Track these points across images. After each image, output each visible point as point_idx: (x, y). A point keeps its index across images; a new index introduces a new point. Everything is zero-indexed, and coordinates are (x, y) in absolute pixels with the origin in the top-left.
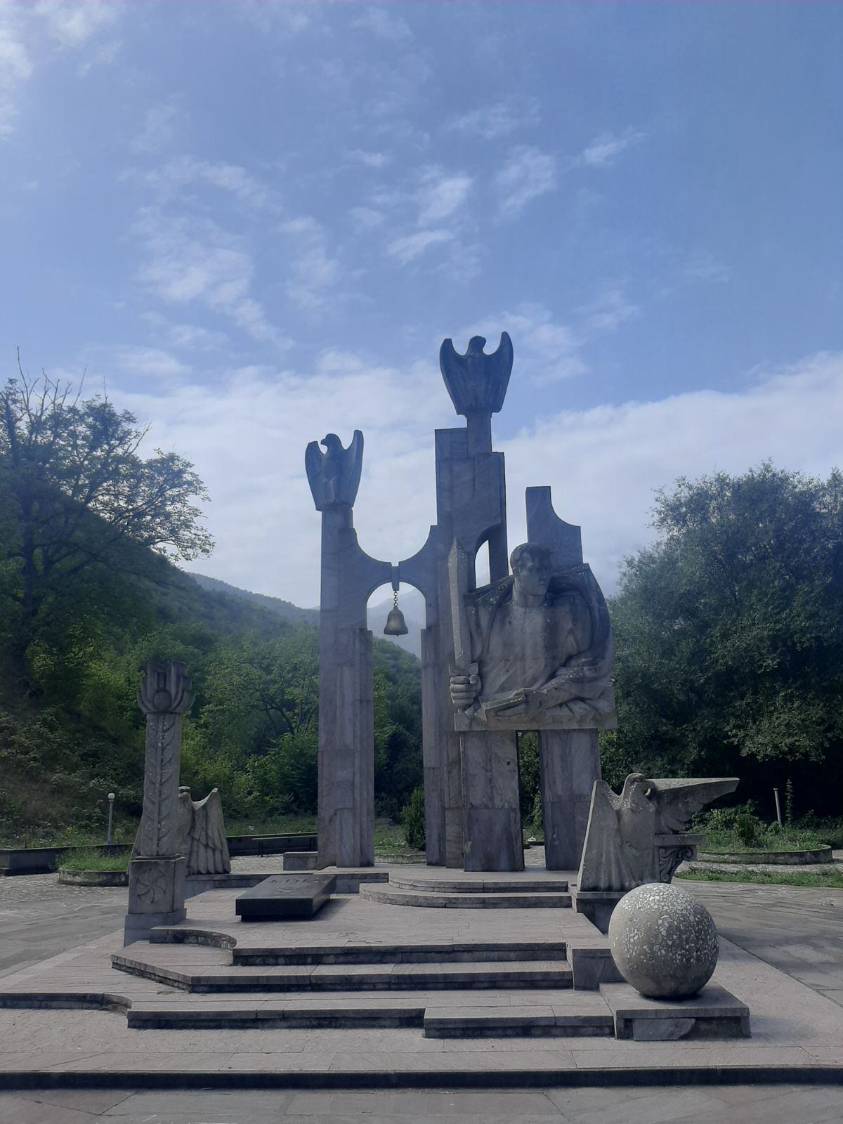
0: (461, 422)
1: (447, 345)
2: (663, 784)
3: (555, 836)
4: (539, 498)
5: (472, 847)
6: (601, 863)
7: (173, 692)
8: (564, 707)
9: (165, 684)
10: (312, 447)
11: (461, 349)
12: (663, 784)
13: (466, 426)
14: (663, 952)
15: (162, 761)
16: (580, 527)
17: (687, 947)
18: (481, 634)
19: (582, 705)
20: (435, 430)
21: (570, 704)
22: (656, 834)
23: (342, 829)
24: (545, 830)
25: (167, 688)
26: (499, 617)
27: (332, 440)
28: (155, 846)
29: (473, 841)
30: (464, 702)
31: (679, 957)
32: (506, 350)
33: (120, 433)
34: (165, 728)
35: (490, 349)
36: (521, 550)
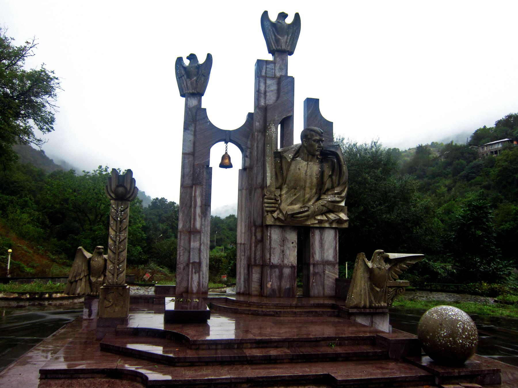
0: (270, 57)
1: (265, 14)
2: (393, 256)
3: (314, 281)
10: (179, 60)
11: (273, 17)
12: (393, 256)
14: (461, 341)
15: (120, 229)
16: (332, 123)
17: (472, 338)
27: (192, 57)
29: (272, 282)
31: (468, 344)
33: (4, 38)
34: (122, 209)
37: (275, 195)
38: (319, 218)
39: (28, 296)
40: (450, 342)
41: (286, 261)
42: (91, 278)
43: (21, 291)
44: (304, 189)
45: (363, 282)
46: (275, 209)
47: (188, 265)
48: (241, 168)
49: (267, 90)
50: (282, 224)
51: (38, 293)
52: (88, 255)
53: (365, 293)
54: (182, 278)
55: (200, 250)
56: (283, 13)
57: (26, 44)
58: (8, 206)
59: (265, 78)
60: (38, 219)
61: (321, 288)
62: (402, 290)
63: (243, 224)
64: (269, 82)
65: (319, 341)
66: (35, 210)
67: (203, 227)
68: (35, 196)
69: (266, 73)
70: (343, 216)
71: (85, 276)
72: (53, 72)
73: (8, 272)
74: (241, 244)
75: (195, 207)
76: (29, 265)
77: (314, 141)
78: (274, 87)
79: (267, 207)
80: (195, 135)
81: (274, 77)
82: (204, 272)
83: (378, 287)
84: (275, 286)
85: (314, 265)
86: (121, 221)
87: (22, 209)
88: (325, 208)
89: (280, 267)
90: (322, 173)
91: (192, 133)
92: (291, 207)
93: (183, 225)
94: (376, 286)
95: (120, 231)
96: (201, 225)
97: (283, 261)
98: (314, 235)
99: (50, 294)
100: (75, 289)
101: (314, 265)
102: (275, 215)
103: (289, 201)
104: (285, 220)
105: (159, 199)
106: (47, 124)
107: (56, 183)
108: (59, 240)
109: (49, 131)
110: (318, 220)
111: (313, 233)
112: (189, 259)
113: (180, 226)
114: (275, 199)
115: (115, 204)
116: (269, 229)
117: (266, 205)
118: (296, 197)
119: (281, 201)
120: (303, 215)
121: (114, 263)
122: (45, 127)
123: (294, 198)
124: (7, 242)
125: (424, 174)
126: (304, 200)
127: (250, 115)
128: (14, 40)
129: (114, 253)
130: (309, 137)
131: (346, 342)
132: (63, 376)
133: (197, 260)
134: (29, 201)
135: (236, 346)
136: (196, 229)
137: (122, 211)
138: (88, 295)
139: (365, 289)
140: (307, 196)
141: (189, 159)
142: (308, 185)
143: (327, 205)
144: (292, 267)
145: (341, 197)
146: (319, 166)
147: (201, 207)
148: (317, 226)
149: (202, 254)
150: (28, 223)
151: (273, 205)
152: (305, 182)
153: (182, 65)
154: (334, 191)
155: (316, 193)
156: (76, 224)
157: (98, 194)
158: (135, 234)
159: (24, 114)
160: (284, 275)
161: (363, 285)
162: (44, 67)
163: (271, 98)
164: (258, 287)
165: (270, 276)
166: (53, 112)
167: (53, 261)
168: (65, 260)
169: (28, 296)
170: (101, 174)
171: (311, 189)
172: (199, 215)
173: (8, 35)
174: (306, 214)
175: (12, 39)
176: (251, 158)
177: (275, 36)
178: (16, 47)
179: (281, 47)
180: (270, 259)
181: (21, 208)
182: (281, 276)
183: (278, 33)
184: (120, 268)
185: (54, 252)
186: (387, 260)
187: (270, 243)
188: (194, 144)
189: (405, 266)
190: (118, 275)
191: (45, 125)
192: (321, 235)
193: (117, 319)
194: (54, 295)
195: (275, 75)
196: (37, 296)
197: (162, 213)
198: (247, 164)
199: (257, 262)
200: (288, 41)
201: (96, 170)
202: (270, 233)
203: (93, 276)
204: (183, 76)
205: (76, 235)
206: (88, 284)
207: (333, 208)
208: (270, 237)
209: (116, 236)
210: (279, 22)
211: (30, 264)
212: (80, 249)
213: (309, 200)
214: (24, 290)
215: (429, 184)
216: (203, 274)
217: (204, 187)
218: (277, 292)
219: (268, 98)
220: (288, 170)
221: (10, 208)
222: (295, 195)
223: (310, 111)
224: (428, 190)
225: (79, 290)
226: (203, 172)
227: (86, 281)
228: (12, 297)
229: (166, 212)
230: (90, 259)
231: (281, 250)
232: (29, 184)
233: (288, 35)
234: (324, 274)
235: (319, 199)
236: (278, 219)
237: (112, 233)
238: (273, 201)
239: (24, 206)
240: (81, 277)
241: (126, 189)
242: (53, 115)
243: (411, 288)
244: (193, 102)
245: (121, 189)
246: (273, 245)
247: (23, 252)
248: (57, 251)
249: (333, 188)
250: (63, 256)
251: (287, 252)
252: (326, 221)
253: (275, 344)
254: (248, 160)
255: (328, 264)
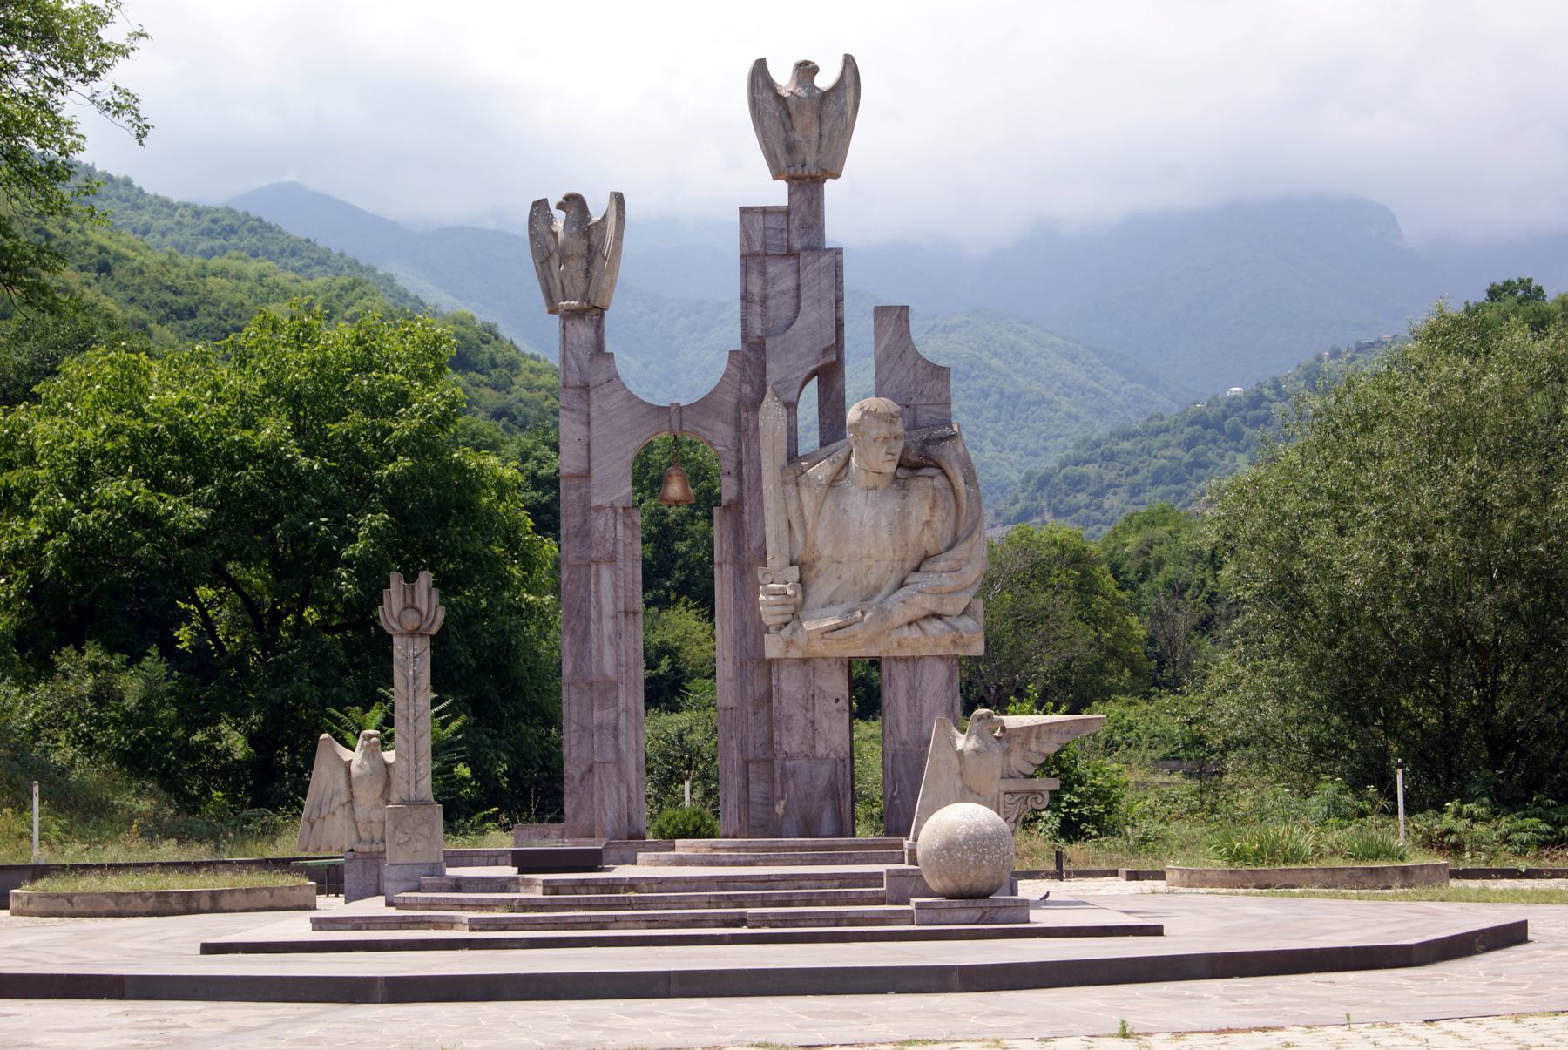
0: (777, 193)
1: (760, 68)
5: (785, 808)
7: (424, 608)
8: (914, 626)
9: (413, 601)
10: (540, 206)
11: (783, 77)
13: (786, 203)
19: (937, 624)
21: (921, 623)
22: (1002, 778)
23: (602, 789)
25: (417, 604)
26: (829, 502)
27: (574, 203)
28: (412, 790)
30: (780, 619)
32: (849, 79)
35: (824, 81)
54: (579, 804)
55: (616, 729)
56: (806, 63)
64: (773, 269)
75: (599, 620)
93: (575, 667)
141: (578, 489)
149: (622, 739)
165: (782, 787)
172: (609, 637)
223: (883, 345)
231: (806, 718)
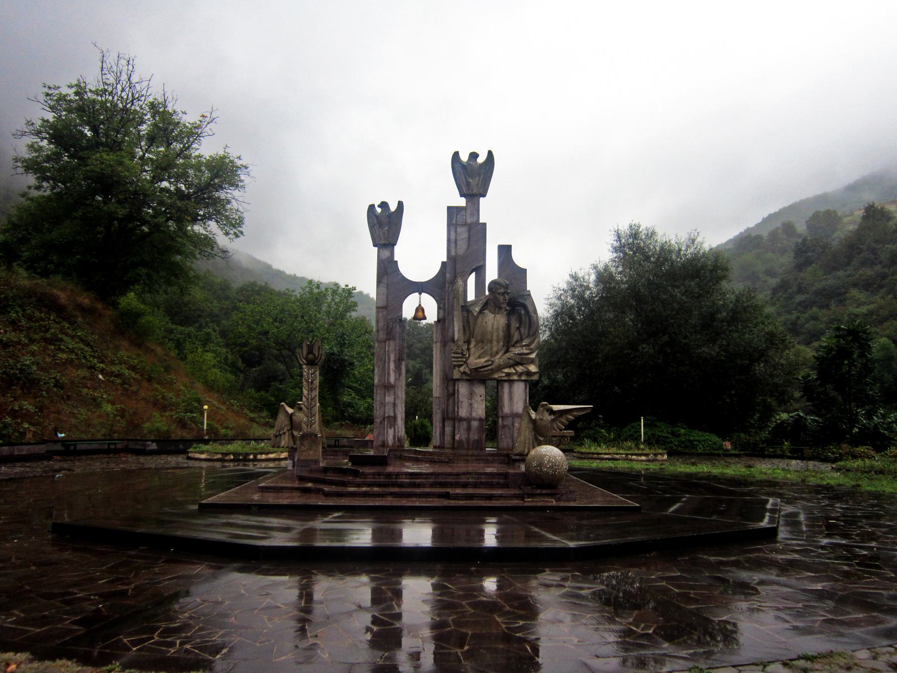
0: (462, 202)
1: (456, 155)
2: (556, 407)
4: (505, 251)
6: (694, 653)
10: (372, 207)
11: (464, 158)
16: (525, 270)
18: (469, 327)
20: (449, 208)
24: (486, 380)
27: (384, 205)
36: (493, 283)
37: (462, 350)
38: (506, 370)
39: (232, 457)
40: (538, 470)
41: (474, 414)
42: (294, 432)
43: (224, 451)
44: (491, 342)
45: (527, 432)
46: (463, 363)
47: (384, 419)
48: (436, 320)
49: (458, 238)
50: (468, 378)
51: (242, 454)
52: (290, 411)
53: (529, 442)
54: (379, 433)
57: (201, 119)
58: (185, 342)
59: (456, 225)
60: (226, 359)
61: (510, 440)
62: (566, 440)
63: (438, 377)
65: (460, 475)
66: (220, 347)
67: (397, 382)
68: (219, 323)
69: (456, 221)
70: (533, 368)
71: (288, 430)
72: (239, 158)
73: (205, 432)
74: (436, 397)
75: (389, 362)
76: (224, 426)
77: (499, 294)
78: (465, 235)
79: (454, 361)
80: (387, 288)
81: (465, 224)
82: (400, 426)
83: (541, 437)
84: (464, 438)
85: (503, 417)
86: (312, 382)
87: (204, 345)
88: (511, 361)
89: (469, 420)
90: (508, 326)
91: (386, 286)
92: (478, 361)
93: (379, 380)
94: (539, 436)
95: (311, 390)
96: (396, 380)
97: (471, 414)
98: (503, 388)
99: (255, 455)
100: (280, 442)
101: (503, 417)
102: (462, 369)
103: (477, 355)
104: (471, 374)
105: (408, 319)
106: (235, 227)
107: (250, 309)
108: (258, 391)
109: (237, 236)
110: (505, 373)
111: (502, 386)
112: (384, 413)
113: (376, 381)
114: (462, 354)
115: (306, 368)
116: (457, 383)
117: (453, 359)
118: (483, 350)
119: (469, 355)
120: (486, 369)
121: (307, 417)
122: (232, 232)
123: (482, 351)
124: (195, 396)
125: (876, 258)
126: (492, 353)
127: (443, 263)
128: (186, 114)
129: (308, 408)
130: (494, 290)
131: (483, 476)
132: (272, 491)
133: (392, 414)
134: (213, 332)
135: (394, 477)
136: (390, 383)
137: (312, 374)
138: (291, 448)
139: (529, 439)
140: (495, 349)
142: (495, 338)
143: (514, 358)
144: (480, 420)
145: (530, 349)
146: (505, 319)
147: (395, 361)
148: (506, 378)
150: (214, 366)
151: (460, 359)
152: (492, 336)
153: (373, 213)
154: (522, 343)
155: (503, 346)
156: (282, 367)
157: (309, 323)
158: (364, 381)
159: (204, 215)
160: (473, 428)
161: (527, 435)
162: (227, 150)
163: (462, 247)
164: (451, 440)
166: (241, 209)
167: (252, 420)
168: (267, 420)
169: (232, 457)
170: (311, 292)
171: (498, 342)
173: (178, 108)
174: (489, 368)
175: (183, 113)
176: (444, 310)
177: (466, 178)
178: (189, 123)
179: (472, 191)
180: (458, 412)
181: (202, 344)
182: (469, 429)
183: (468, 175)
184: (312, 420)
185: (252, 408)
186: (552, 412)
187: (458, 396)
188: (387, 296)
189: (571, 417)
190: (311, 426)
191: (232, 229)
192: (511, 387)
193: (311, 460)
194: (259, 457)
195: (466, 222)
196: (241, 457)
197: (414, 343)
198: (441, 316)
199: (450, 415)
200: (480, 183)
201: (304, 287)
202: (458, 387)
203: (295, 430)
204: (376, 225)
205: (281, 382)
206: (291, 438)
207: (521, 361)
208: (458, 391)
209: (309, 394)
210: (469, 164)
211: (225, 425)
212: (283, 405)
213: (497, 353)
214: (227, 451)
215: (884, 276)
216: (398, 428)
217: (398, 341)
218: (465, 445)
219: (458, 246)
220: (475, 324)
221: (188, 346)
222: (483, 348)
223: (502, 259)
224: (881, 287)
225: (283, 444)
226: (396, 326)
227: (289, 435)
228: (216, 458)
229: (420, 341)
230: (292, 414)
232: (209, 305)
233: (480, 176)
234: (514, 427)
235: (507, 351)
236: (464, 373)
237: (305, 392)
238: (460, 355)
239: (206, 341)
240: (285, 431)
241: (315, 355)
242: (242, 213)
243: (733, 452)
244: (386, 253)
245: (311, 356)
246: (461, 399)
247: (214, 408)
248: (256, 407)
249: (522, 340)
250: (264, 414)
251: (475, 405)
252: (515, 374)
253: (425, 476)
254: (441, 311)
255: (517, 417)
